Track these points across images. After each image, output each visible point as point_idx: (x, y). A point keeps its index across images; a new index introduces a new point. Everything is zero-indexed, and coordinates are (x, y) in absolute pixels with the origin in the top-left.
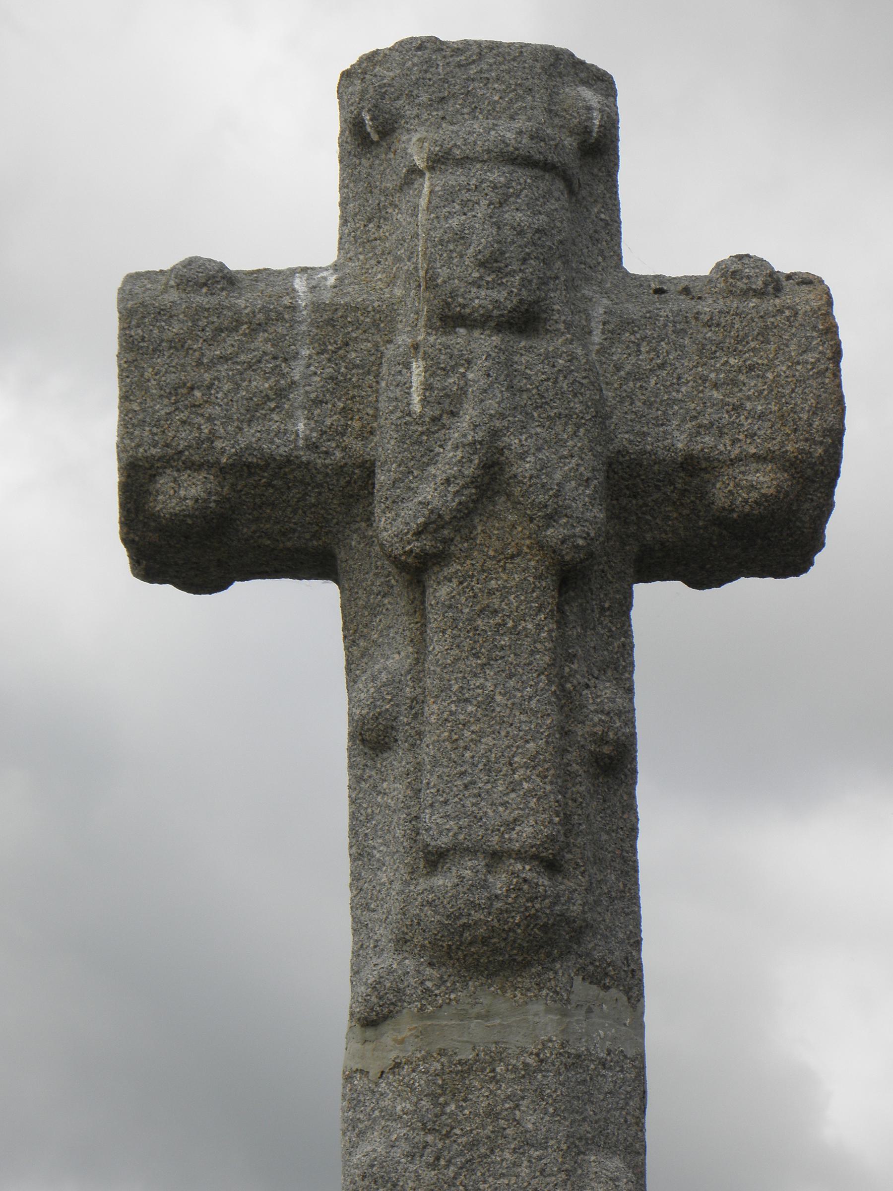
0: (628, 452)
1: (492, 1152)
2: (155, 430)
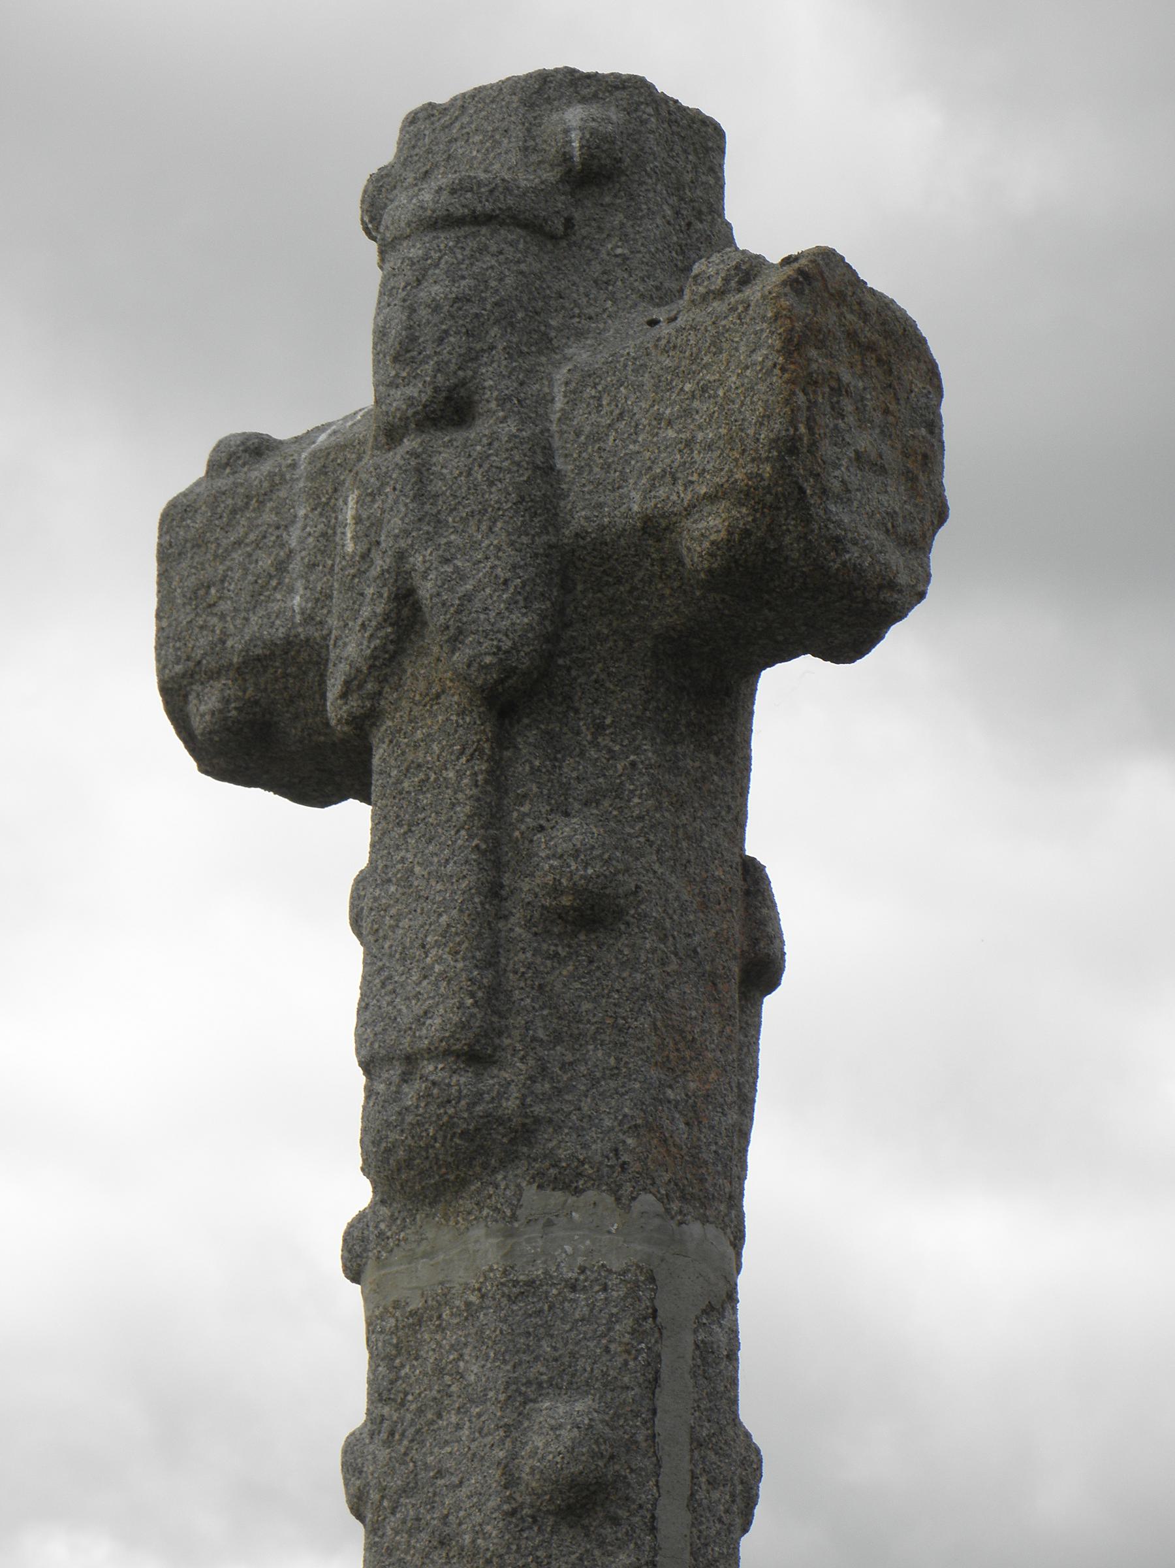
0: (587, 532)
1: (440, 1416)
2: (178, 645)
